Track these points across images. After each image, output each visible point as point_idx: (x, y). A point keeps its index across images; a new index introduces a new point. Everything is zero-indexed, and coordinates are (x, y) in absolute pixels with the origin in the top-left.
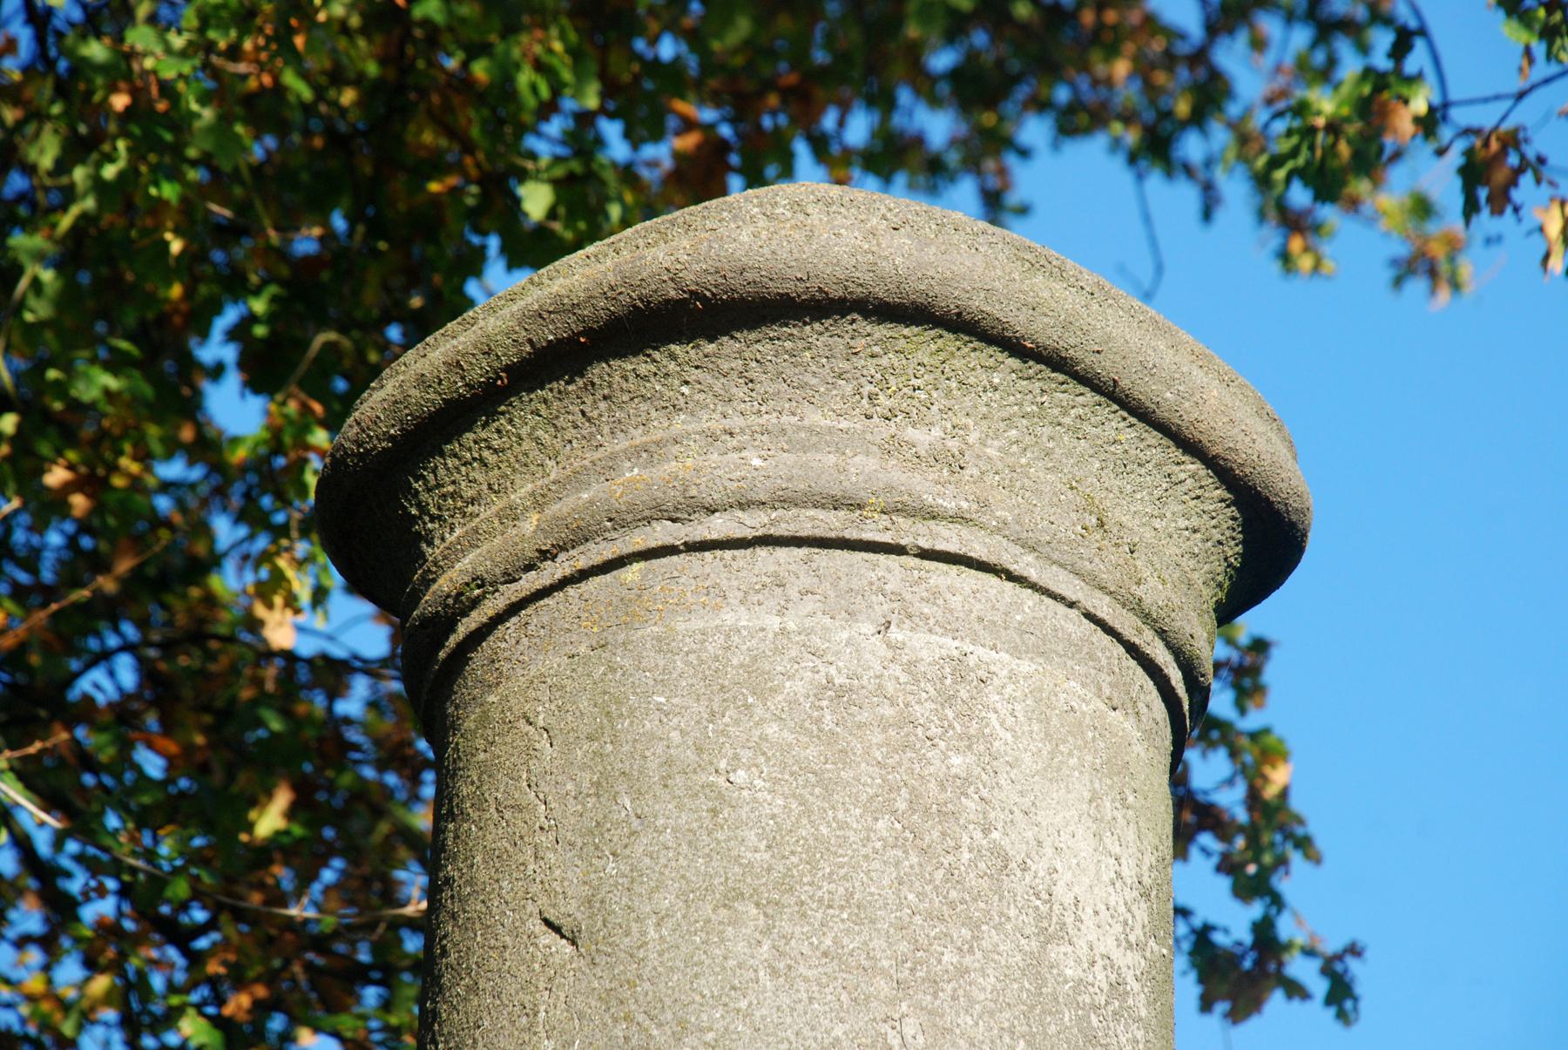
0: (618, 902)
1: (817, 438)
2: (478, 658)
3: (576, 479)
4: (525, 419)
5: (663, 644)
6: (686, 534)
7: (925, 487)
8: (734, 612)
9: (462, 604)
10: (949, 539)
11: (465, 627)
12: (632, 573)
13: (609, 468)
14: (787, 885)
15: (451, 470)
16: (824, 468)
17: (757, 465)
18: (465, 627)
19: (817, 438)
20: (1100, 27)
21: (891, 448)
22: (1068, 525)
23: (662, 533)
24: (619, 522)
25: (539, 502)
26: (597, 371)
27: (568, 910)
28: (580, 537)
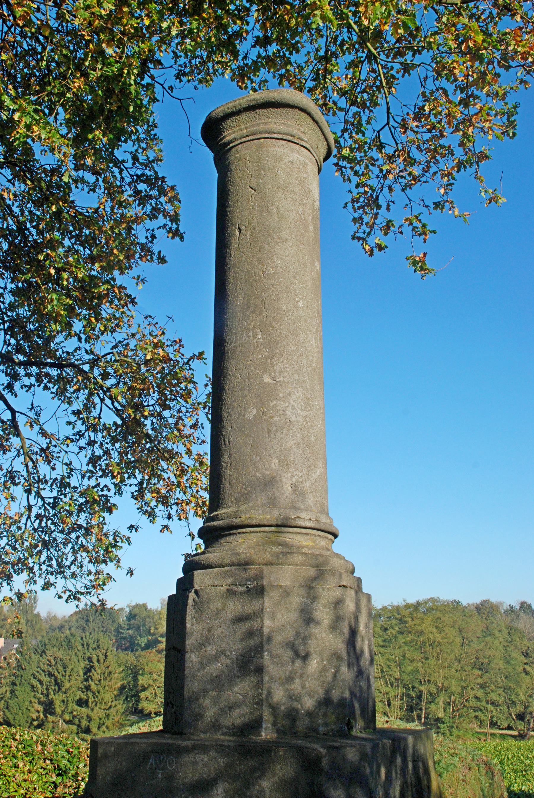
0: (262, 186)
1: (289, 126)
2: (233, 150)
3: (253, 126)
4: (244, 116)
5: (267, 151)
6: (270, 136)
7: (302, 136)
8: (278, 148)
9: (231, 141)
10: (304, 144)
11: (231, 145)
12: (262, 140)
13: (259, 125)
14: (286, 187)
15: (229, 122)
16: (290, 130)
17: (281, 128)
18: (231, 145)
19: (289, 126)
20: (82, 152)
21: (299, 129)
22: (315, 147)
23: (267, 135)
24: (261, 133)
25: (246, 128)
26: (258, 111)
27: (254, 186)
28: (254, 134)
